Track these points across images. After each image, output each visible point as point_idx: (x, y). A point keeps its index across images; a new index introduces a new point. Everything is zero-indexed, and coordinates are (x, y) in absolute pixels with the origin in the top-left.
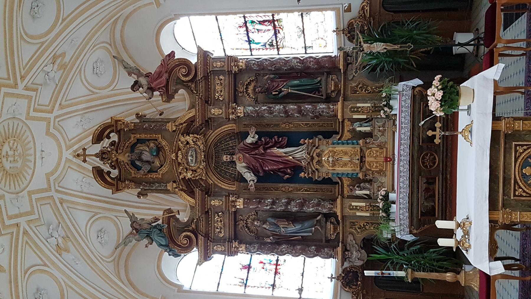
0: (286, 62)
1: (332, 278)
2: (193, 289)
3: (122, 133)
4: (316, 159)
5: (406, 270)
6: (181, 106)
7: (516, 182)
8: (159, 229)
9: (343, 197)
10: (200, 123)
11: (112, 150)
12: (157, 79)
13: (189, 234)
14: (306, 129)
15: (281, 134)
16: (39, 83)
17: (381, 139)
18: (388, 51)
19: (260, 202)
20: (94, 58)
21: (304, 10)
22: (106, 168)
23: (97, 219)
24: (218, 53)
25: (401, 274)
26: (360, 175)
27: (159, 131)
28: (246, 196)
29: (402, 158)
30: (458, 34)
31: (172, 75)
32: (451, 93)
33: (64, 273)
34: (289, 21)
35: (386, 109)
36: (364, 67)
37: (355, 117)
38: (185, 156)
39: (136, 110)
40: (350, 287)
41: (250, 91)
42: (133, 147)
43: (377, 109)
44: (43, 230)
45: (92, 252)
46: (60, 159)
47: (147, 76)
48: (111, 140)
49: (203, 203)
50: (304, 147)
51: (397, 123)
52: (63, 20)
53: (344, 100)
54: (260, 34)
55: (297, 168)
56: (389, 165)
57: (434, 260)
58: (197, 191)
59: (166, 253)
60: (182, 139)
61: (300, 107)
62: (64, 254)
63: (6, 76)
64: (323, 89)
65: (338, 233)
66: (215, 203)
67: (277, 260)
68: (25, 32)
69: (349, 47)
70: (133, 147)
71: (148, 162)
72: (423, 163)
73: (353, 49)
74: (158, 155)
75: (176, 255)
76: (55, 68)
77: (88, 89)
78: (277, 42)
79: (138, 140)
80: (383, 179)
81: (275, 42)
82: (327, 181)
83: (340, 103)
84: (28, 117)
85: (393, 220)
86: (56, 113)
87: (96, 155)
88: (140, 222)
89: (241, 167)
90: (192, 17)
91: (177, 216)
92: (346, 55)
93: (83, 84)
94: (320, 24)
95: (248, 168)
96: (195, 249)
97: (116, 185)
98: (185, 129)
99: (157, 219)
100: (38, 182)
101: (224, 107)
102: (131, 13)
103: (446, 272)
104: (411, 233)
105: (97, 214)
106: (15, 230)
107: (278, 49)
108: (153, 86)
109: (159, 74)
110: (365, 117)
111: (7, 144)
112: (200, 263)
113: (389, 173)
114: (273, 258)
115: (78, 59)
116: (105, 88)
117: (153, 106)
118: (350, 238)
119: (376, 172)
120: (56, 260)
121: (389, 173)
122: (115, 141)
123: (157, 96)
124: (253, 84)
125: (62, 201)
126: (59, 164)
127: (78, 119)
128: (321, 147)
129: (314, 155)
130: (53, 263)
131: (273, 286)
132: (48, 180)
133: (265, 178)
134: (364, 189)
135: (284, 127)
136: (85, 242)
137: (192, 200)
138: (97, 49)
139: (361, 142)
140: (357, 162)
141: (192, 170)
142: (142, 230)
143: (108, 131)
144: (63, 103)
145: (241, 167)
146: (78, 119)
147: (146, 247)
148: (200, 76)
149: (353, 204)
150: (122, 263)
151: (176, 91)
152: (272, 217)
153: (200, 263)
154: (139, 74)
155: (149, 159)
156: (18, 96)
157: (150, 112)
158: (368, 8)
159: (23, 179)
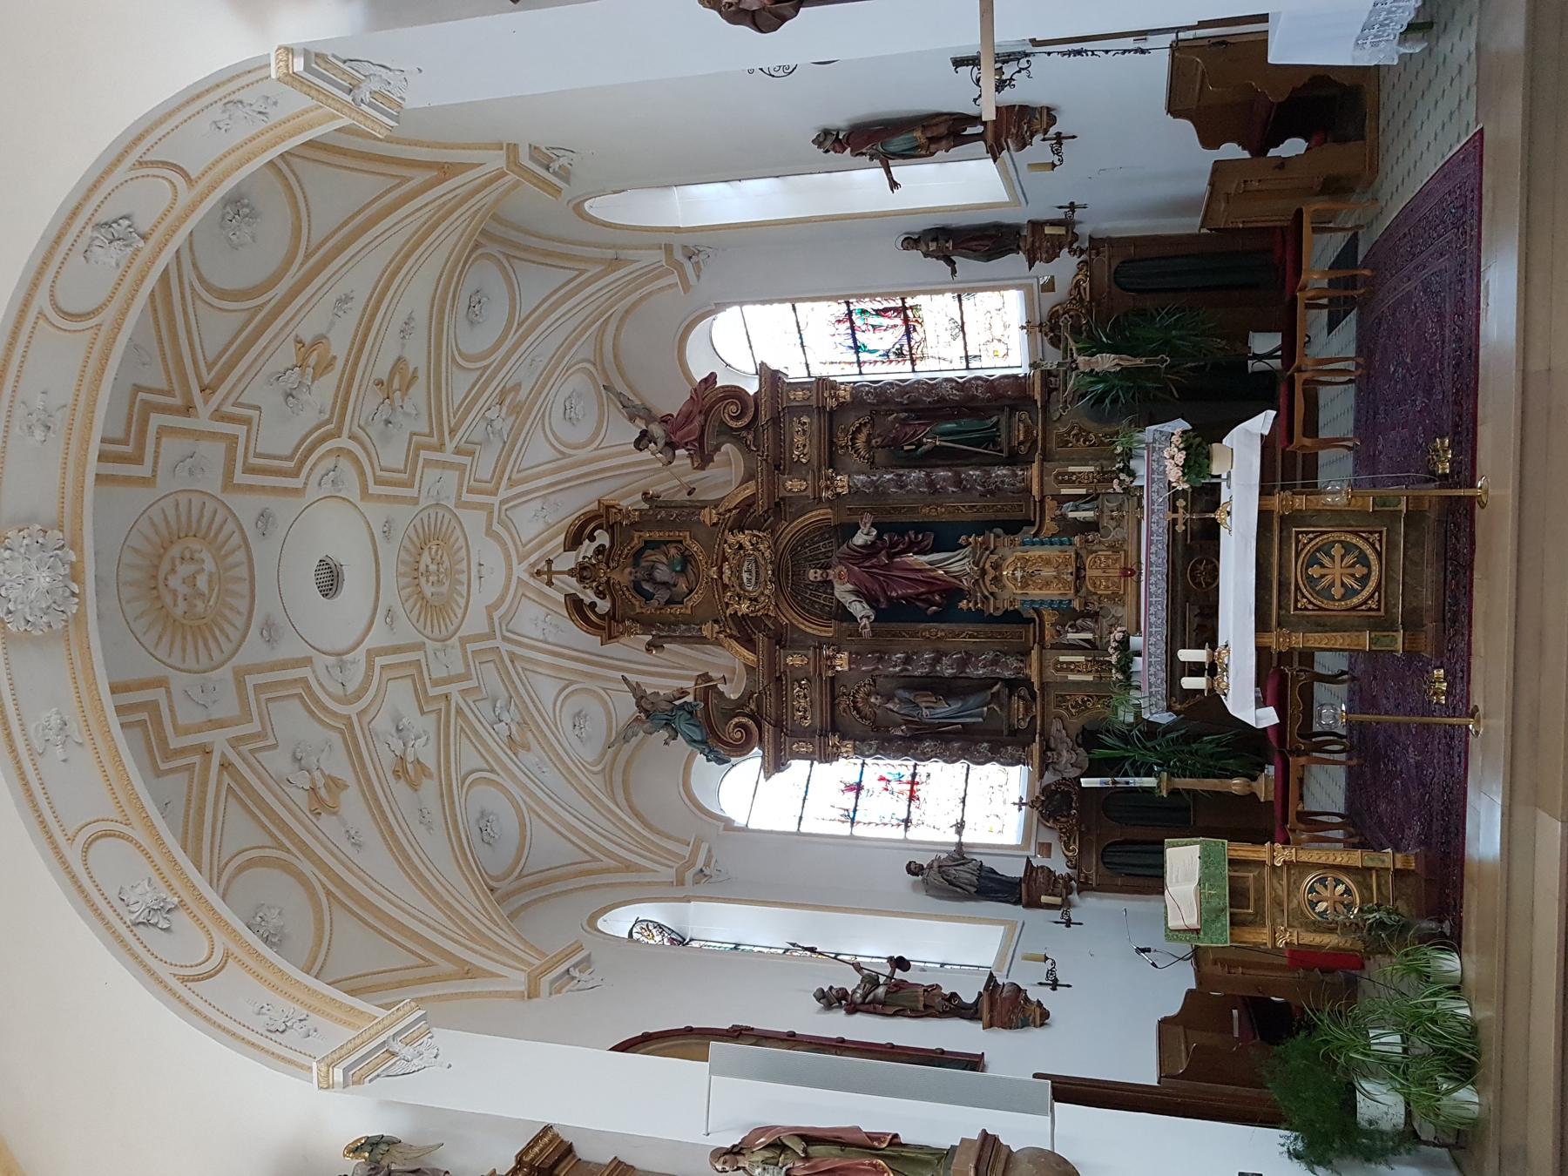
0: (930, 387)
1: (1020, 804)
4: (991, 573)
5: (1157, 775)
6: (726, 477)
7: (1297, 587)
9: (1043, 647)
12: (682, 427)
13: (744, 720)
14: (970, 516)
15: (920, 527)
17: (1115, 534)
18: (1124, 369)
19: (880, 659)
20: (567, 390)
21: (964, 290)
22: (588, 596)
24: (796, 373)
25: (1149, 782)
26: (1076, 604)
28: (854, 648)
29: (1154, 569)
30: (1257, 335)
31: (716, 417)
32: (1197, 455)
33: (524, 787)
34: (936, 310)
35: (1123, 476)
36: (1083, 396)
37: (1064, 491)
40: (1056, 820)
41: (860, 443)
42: (638, 555)
43: (1106, 477)
44: (486, 707)
46: (509, 578)
47: (664, 420)
49: (772, 662)
50: (967, 550)
51: (1145, 502)
52: (520, 325)
53: (1044, 460)
54: (879, 334)
55: (952, 593)
56: (1131, 581)
57: (1212, 755)
58: (760, 638)
60: (731, 539)
61: (957, 474)
62: (522, 752)
63: (427, 431)
64: (1003, 439)
65: (1034, 717)
66: (794, 660)
67: (914, 775)
69: (1053, 358)
70: (638, 555)
71: (665, 583)
72: (1193, 578)
73: (1059, 365)
74: (683, 571)
78: (911, 348)
79: (646, 542)
80: (1119, 611)
81: (906, 348)
82: (1013, 617)
83: (1035, 466)
84: (228, 484)
85: (1138, 688)
86: (503, 493)
87: (571, 573)
89: (843, 592)
90: (746, 308)
91: (721, 687)
92: (1047, 375)
94: (994, 313)
95: (857, 593)
97: (607, 627)
99: (684, 693)
100: (475, 623)
101: (810, 477)
102: (635, 305)
103: (1231, 778)
104: (1169, 708)
105: (572, 682)
106: (443, 705)
107: (913, 362)
109: (687, 417)
110: (1083, 491)
113: (1130, 599)
114: (903, 767)
116: (584, 446)
118: (1056, 725)
119: (1107, 596)
121: (1130, 599)
123: (682, 457)
124: (865, 431)
127: (537, 504)
128: (1001, 551)
129: (987, 566)
130: (505, 768)
131: (907, 822)
132: (491, 618)
133: (891, 612)
134: (1083, 630)
135: (927, 513)
139: (1076, 539)
140: (1070, 578)
142: (658, 714)
143: (592, 526)
145: (843, 592)
146: (537, 504)
148: (764, 418)
149: (1062, 659)
151: (717, 449)
152: (905, 688)
154: (649, 416)
155: (666, 579)
156: (445, 465)
158: (1087, 285)
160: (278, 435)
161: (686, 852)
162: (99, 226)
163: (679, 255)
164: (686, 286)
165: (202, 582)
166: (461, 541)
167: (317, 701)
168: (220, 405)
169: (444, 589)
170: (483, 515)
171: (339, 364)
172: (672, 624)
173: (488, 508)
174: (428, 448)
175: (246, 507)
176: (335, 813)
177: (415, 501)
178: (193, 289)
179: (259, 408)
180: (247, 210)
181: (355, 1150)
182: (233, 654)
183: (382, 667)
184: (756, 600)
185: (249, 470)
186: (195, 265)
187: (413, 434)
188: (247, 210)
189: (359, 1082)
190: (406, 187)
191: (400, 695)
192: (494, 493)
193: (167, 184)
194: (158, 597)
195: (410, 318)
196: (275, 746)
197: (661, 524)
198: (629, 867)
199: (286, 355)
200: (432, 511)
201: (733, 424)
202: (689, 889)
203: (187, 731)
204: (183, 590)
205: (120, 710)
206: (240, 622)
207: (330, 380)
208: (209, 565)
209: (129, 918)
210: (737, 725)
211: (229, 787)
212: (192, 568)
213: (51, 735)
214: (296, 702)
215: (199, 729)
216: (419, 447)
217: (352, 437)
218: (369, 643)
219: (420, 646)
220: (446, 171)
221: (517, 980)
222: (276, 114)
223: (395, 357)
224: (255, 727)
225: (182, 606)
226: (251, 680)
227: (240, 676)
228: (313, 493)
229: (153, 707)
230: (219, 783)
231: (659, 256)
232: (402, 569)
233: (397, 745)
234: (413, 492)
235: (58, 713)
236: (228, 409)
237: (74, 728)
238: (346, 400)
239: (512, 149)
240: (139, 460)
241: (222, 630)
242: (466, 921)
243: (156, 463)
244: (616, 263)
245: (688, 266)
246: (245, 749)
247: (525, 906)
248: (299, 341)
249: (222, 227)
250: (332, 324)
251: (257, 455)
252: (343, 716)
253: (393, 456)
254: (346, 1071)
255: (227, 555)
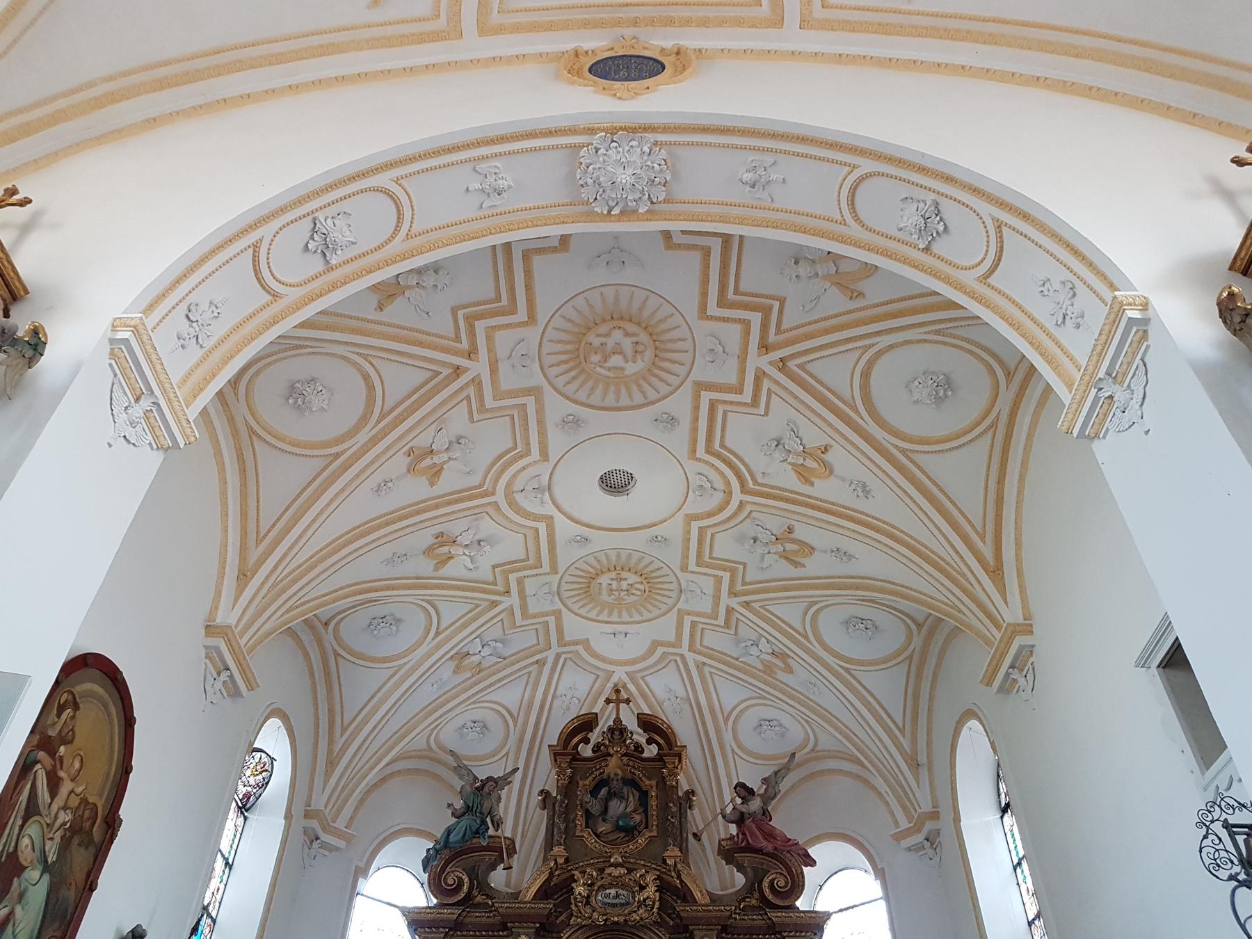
2: (359, 902)
3: (658, 765)
6: (714, 878)
8: (480, 831)
10: (682, 914)
11: (628, 747)
12: (760, 829)
13: (465, 888)
16: (739, 630)
20: (786, 720)
22: (595, 737)
23: (506, 721)
27: (664, 832)
31: (771, 862)
33: (419, 664)
38: (617, 883)
39: (698, 790)
42: (633, 783)
44: (496, 632)
45: (450, 711)
46: (611, 662)
47: (765, 812)
48: (644, 745)
49: (523, 918)
52: (847, 670)
59: (431, 845)
60: (650, 878)
62: (453, 664)
63: (748, 579)
68: (818, 611)
70: (633, 783)
71: (605, 810)
74: (618, 828)
75: (426, 863)
76: (764, 656)
77: (734, 708)
79: (646, 793)
84: (700, 386)
87: (618, 720)
88: (494, 795)
93: (741, 703)
96: (435, 901)
97: (565, 751)
98: (669, 883)
99: (497, 825)
100: (574, 627)
102: (874, 788)
105: (515, 721)
106: (500, 588)
108: (748, 822)
109: (770, 835)
111: (639, 579)
112: (406, 912)
115: (784, 693)
117: (711, 821)
120: (445, 649)
122: (643, 751)
123: (727, 829)
125: (541, 663)
126: (604, 660)
130: (438, 647)
136: (469, 698)
137: (530, 895)
138: (803, 726)
141: (588, 897)
142: (479, 799)
143: (661, 741)
144: (707, 669)
147: (449, 805)
148: (773, 914)
150: (424, 765)
151: (741, 869)
153: (406, 912)
154: (767, 798)
155: (611, 811)
156: (717, 598)
157: (696, 818)
159: (581, 604)
160: (743, 433)
161: (340, 824)
162: (936, 204)
163: (929, 826)
164: (898, 837)
165: (616, 360)
166: (647, 615)
167: (510, 463)
168: (769, 377)
169: (605, 597)
170: (672, 638)
171: (806, 489)
172: (567, 814)
173: (678, 643)
174: (732, 580)
175: (680, 404)
176: (409, 471)
177: (684, 568)
178: (871, 346)
179: (766, 414)
180: (941, 394)
181: (36, 332)
182: (556, 389)
183: (537, 530)
184: (588, 903)
185: (713, 405)
186: (891, 347)
187: (745, 565)
188: (941, 394)
189: (112, 354)
190: (974, 537)
191: (511, 546)
192: (691, 649)
193: (978, 260)
194: (604, 321)
195: (851, 557)
196: (472, 420)
197: (664, 808)
198: (331, 764)
199: (813, 437)
200: (674, 586)
201: (766, 883)
202: (299, 822)
203: (490, 338)
204: (610, 343)
205: (508, 246)
206: (582, 396)
207: (791, 481)
208: (631, 369)
209: (321, 216)
210: (461, 882)
211: (439, 373)
212: (629, 350)
213: (491, 179)
214: (511, 445)
215: (490, 350)
216: (733, 572)
217: (742, 505)
218: (558, 517)
219: (554, 569)
220: (996, 572)
221: (227, 616)
222: (1066, 335)
223: (814, 544)
224: (489, 402)
225: (597, 342)
226: (530, 401)
227: (536, 392)
228: (692, 467)
229: (512, 310)
230: (444, 364)
231: (926, 807)
232: (624, 555)
233: (466, 539)
234: (692, 566)
235: (510, 187)
236: (766, 384)
237: (496, 200)
238: (774, 498)
239: (1028, 630)
240: (722, 303)
241: (574, 378)
242: (295, 581)
243: (718, 319)
244: (915, 765)
245: (920, 838)
246: (471, 391)
247: (306, 656)
248: (826, 449)
249: (924, 373)
250: (843, 480)
251: (725, 412)
252: (494, 488)
253: (725, 546)
254: (126, 341)
255: (639, 386)
